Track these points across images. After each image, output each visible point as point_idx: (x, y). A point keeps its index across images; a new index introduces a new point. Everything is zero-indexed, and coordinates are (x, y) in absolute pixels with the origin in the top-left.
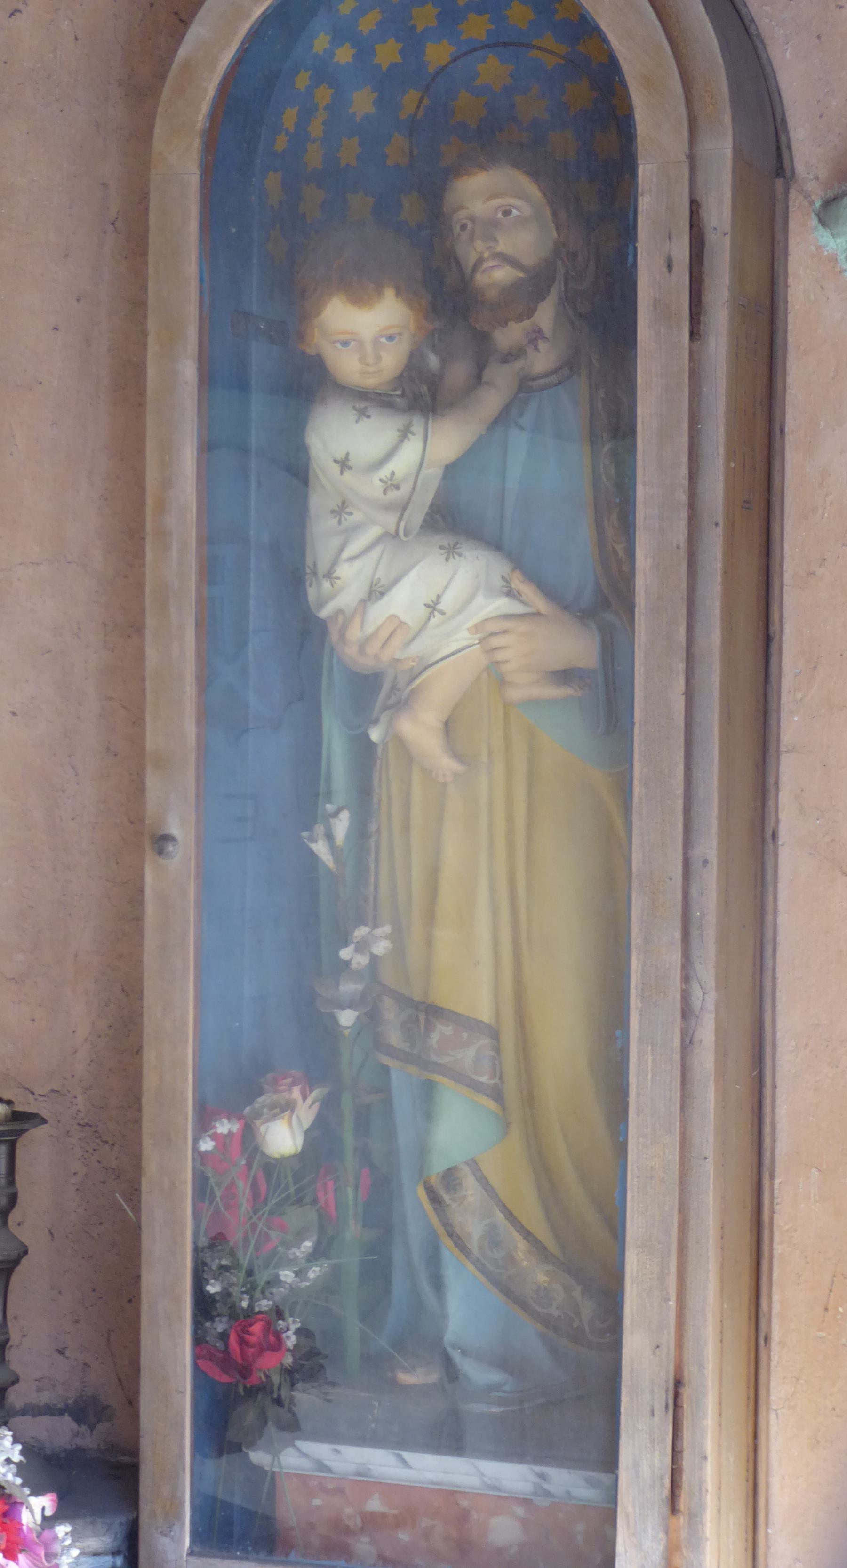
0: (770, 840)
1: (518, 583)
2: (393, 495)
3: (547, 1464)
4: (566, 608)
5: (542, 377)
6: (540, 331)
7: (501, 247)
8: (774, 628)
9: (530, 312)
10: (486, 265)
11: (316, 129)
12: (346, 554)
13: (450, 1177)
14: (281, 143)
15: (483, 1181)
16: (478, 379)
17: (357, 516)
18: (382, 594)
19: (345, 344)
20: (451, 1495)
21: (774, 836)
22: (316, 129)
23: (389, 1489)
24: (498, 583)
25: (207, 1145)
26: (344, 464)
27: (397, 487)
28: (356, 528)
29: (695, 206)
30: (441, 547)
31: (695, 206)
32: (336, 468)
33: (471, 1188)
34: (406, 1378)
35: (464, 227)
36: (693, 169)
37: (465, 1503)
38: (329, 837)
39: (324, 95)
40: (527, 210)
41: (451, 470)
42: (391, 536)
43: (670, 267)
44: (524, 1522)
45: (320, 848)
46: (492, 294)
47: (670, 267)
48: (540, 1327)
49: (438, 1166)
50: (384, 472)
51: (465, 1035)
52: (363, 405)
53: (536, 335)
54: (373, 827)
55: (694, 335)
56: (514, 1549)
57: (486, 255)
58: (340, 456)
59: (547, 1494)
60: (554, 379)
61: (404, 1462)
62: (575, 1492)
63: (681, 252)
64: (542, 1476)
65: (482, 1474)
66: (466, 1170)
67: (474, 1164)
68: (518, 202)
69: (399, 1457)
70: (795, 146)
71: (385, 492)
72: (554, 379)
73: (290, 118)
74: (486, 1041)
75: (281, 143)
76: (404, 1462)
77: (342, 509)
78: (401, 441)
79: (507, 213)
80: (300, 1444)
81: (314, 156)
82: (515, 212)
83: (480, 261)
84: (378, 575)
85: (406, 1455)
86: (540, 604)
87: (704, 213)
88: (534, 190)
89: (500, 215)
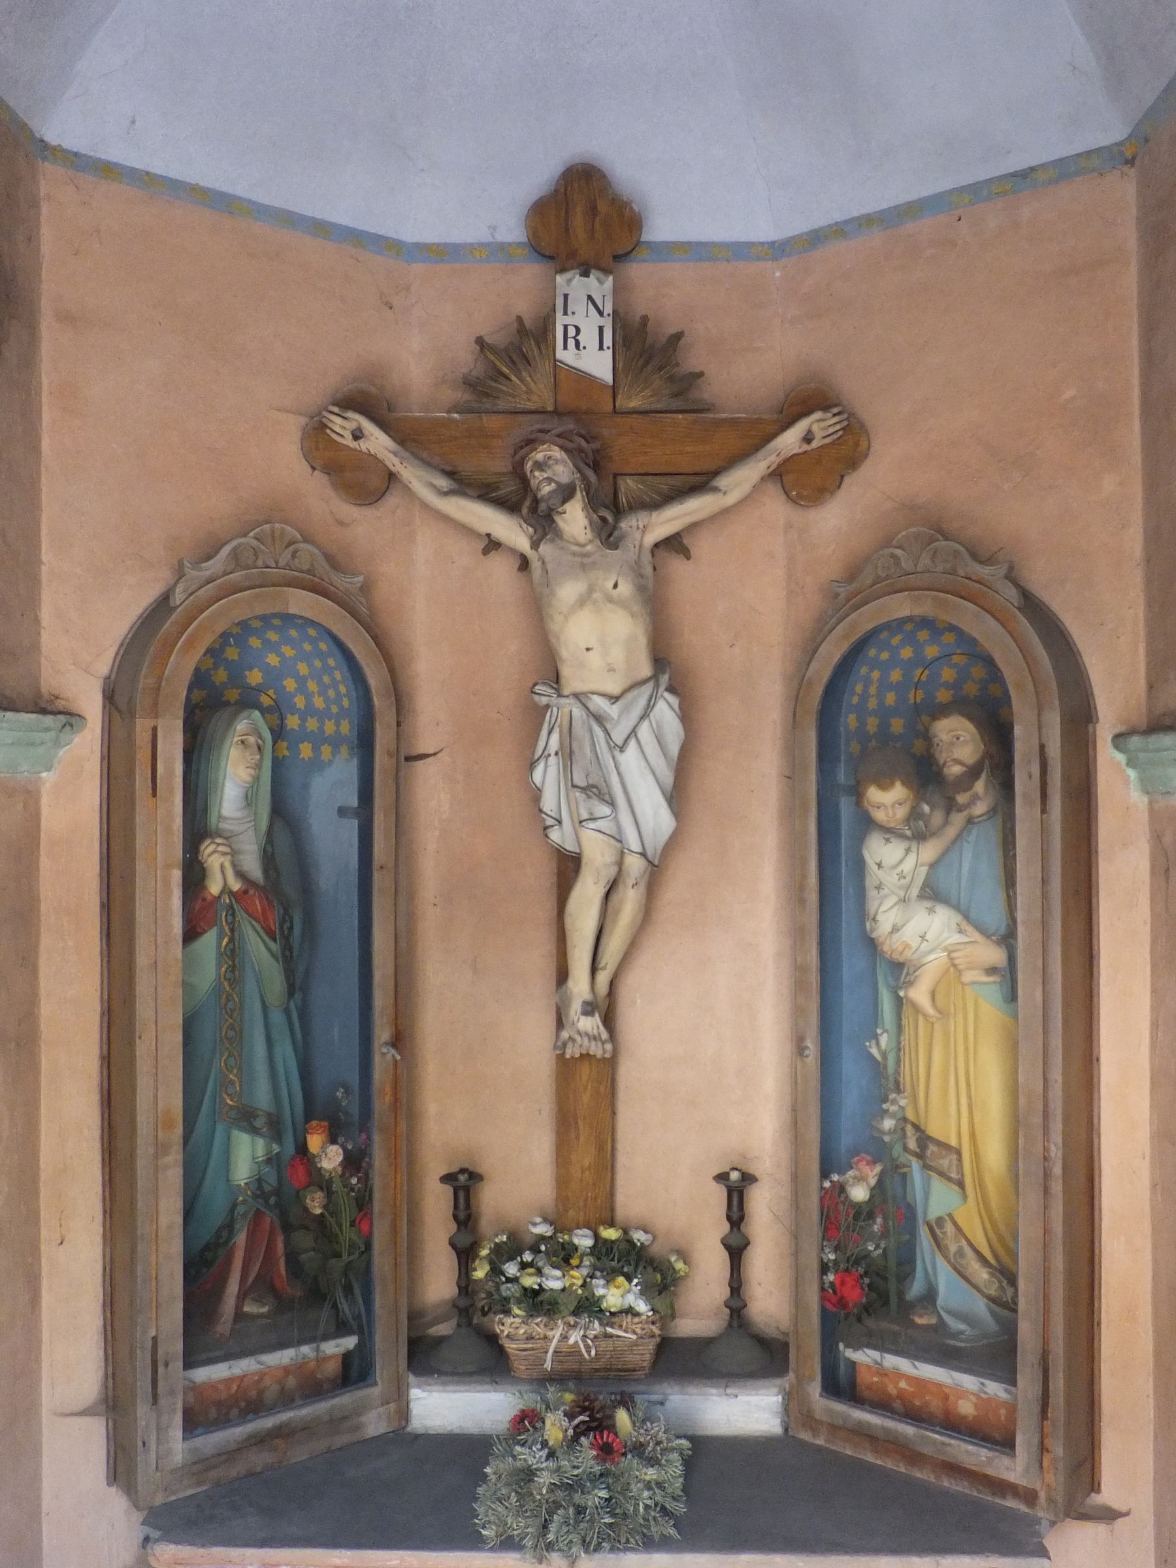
0: (1095, 1061)
1: (965, 926)
2: (903, 881)
3: (985, 1378)
4: (988, 937)
5: (980, 816)
6: (977, 794)
7: (956, 756)
8: (1095, 952)
9: (971, 787)
10: (948, 764)
11: (873, 690)
12: (881, 910)
13: (940, 1221)
14: (855, 700)
15: (955, 1224)
16: (946, 822)
17: (886, 891)
18: (898, 930)
19: (879, 808)
20: (939, 1385)
21: (1098, 1060)
22: (873, 690)
23: (910, 1379)
24: (954, 926)
25: (827, 1184)
26: (879, 865)
27: (904, 878)
28: (886, 896)
29: (1042, 747)
30: (927, 908)
31: (1042, 747)
32: (876, 867)
33: (949, 1228)
34: (919, 1321)
35: (938, 745)
36: (1040, 728)
37: (947, 1391)
38: (878, 1044)
39: (876, 675)
40: (968, 738)
41: (933, 866)
42: (904, 901)
43: (1030, 777)
44: (976, 1405)
45: (874, 1051)
46: (951, 778)
47: (1030, 777)
48: (985, 1300)
49: (933, 1215)
50: (899, 870)
51: (944, 1153)
52: (887, 836)
53: (976, 798)
54: (902, 1038)
55: (1043, 811)
56: (971, 1418)
57: (948, 760)
58: (878, 861)
59: (985, 1393)
60: (984, 818)
61: (916, 1367)
62: (999, 1394)
63: (1036, 770)
64: (982, 1384)
65: (953, 1379)
66: (947, 1218)
67: (950, 1216)
68: (965, 734)
69: (914, 1364)
70: (1099, 708)
71: (899, 880)
72: (984, 818)
73: (859, 688)
74: (955, 1157)
75: (855, 700)
76: (916, 1367)
77: (879, 888)
78: (906, 855)
79: (958, 739)
80: (865, 1350)
81: (872, 704)
82: (962, 739)
83: (945, 763)
84: (897, 921)
85: (917, 1363)
86: (977, 936)
87: (1046, 750)
88: (969, 726)
89: (955, 740)
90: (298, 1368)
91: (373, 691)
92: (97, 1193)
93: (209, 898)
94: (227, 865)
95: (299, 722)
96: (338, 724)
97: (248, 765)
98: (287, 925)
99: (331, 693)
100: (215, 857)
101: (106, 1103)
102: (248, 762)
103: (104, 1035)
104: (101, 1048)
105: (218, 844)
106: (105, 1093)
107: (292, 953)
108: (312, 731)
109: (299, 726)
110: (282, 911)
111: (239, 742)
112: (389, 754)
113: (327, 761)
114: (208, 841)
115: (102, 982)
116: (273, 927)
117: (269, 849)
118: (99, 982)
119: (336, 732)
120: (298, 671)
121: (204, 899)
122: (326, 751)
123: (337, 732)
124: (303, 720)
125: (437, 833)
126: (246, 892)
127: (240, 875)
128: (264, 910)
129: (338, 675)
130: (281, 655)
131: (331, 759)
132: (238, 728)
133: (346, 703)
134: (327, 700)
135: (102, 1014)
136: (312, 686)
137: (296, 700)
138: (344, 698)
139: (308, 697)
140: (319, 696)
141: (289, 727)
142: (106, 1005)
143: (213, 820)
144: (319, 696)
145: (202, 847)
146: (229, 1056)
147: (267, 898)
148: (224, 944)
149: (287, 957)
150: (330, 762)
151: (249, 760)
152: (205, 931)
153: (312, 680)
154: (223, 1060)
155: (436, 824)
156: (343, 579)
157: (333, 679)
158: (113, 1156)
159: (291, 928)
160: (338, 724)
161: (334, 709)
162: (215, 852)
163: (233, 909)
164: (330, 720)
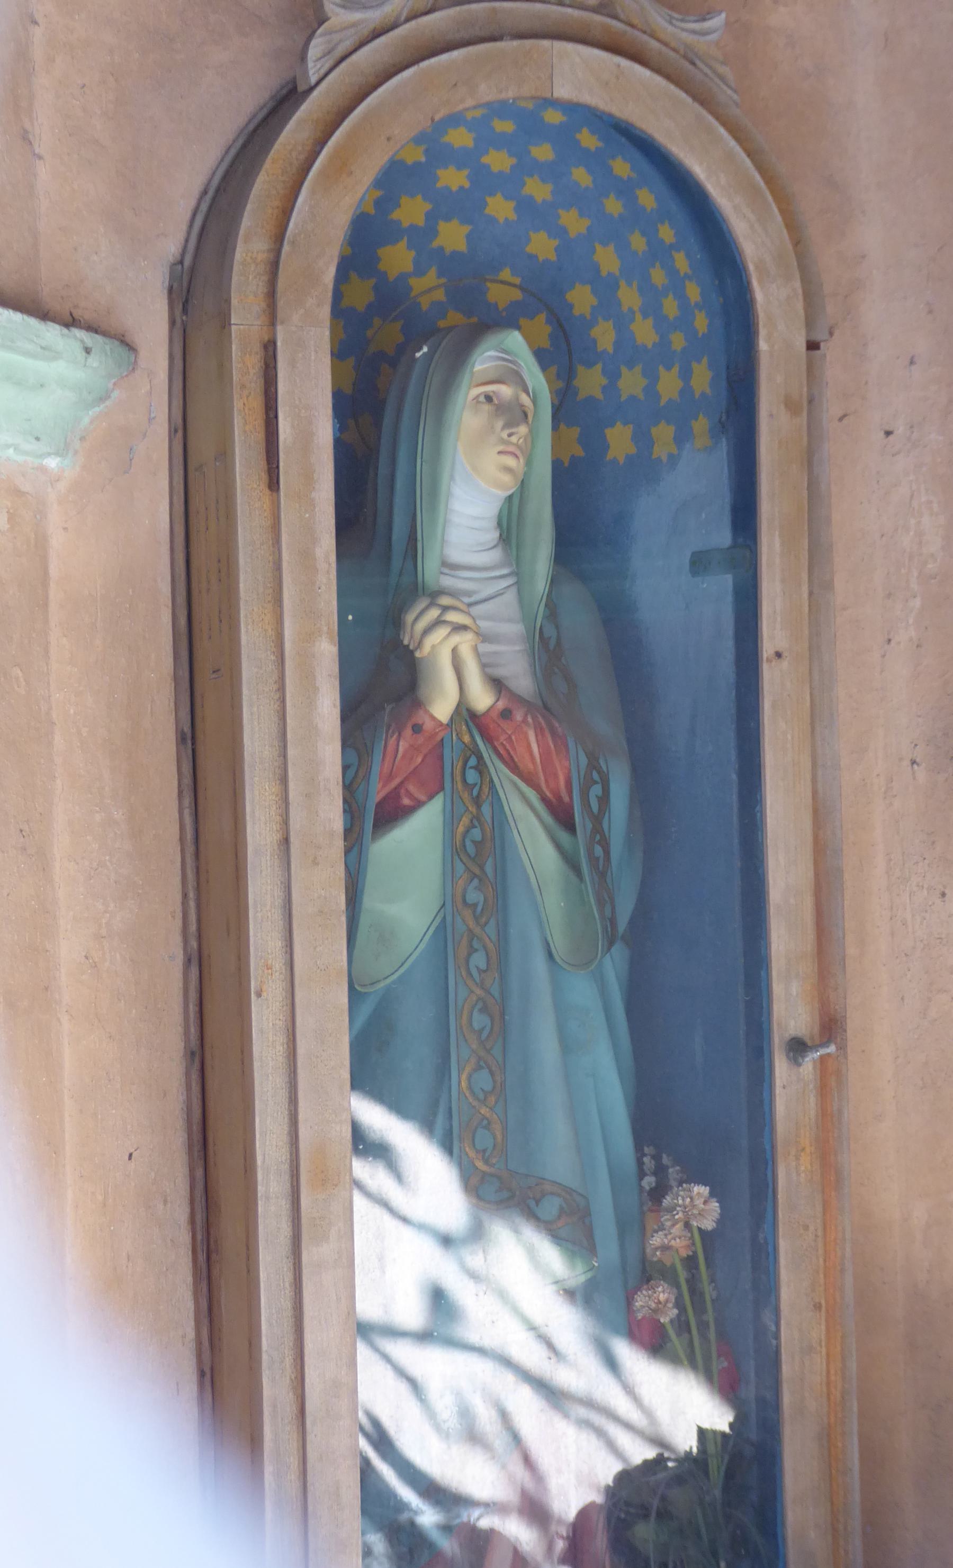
90: (679, 1335)
91: (751, 267)
92: (184, 1336)
93: (428, 725)
94: (466, 653)
95: (605, 381)
96: (686, 374)
97: (501, 448)
98: (596, 790)
99: (670, 307)
100: (440, 633)
101: (197, 1147)
102: (503, 442)
103: (192, 1030)
104: (186, 1033)
105: (445, 609)
106: (196, 1128)
107: (607, 852)
108: (633, 398)
109: (604, 389)
110: (583, 760)
111: (482, 399)
112: (791, 406)
113: (664, 458)
114: (422, 603)
115: (185, 896)
116: (566, 799)
117: (550, 632)
118: (178, 897)
119: (682, 392)
120: (596, 268)
121: (417, 729)
122: (664, 433)
123: (686, 391)
124: (613, 376)
125: (917, 603)
126: (506, 714)
127: (497, 684)
128: (546, 756)
129: (681, 262)
130: (559, 232)
131: (675, 451)
132: (478, 367)
133: (701, 322)
134: (663, 325)
135: (188, 962)
136: (629, 297)
137: (596, 332)
138: (697, 312)
139: (622, 323)
140: (645, 316)
141: (582, 395)
142: (194, 944)
143: (430, 569)
144: (645, 316)
145: (410, 617)
146: (478, 1068)
147: (554, 733)
148: (461, 829)
149: (598, 859)
150: (673, 460)
151: (504, 435)
152: (418, 805)
153: (630, 284)
154: (464, 1077)
155: (914, 586)
156: (678, 24)
157: (672, 272)
158: (214, 1256)
159: (605, 799)
160: (686, 374)
161: (678, 341)
162: (438, 622)
163: (480, 758)
164: (669, 368)
